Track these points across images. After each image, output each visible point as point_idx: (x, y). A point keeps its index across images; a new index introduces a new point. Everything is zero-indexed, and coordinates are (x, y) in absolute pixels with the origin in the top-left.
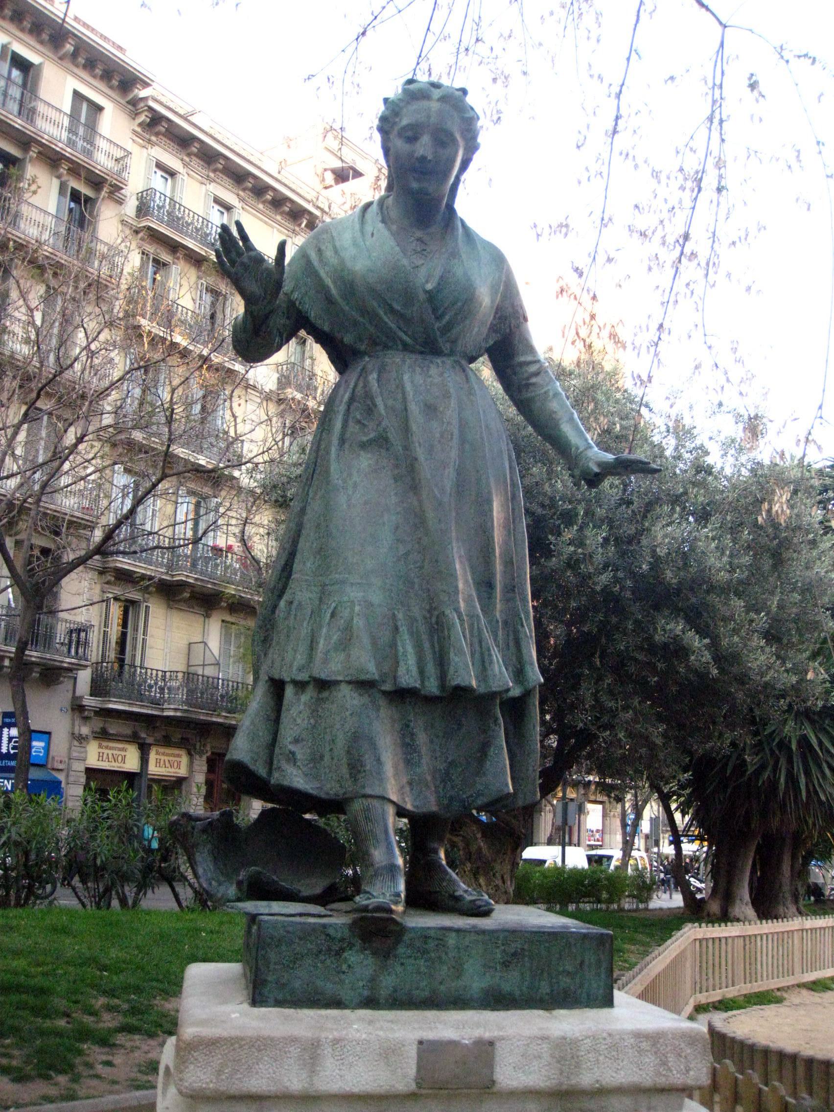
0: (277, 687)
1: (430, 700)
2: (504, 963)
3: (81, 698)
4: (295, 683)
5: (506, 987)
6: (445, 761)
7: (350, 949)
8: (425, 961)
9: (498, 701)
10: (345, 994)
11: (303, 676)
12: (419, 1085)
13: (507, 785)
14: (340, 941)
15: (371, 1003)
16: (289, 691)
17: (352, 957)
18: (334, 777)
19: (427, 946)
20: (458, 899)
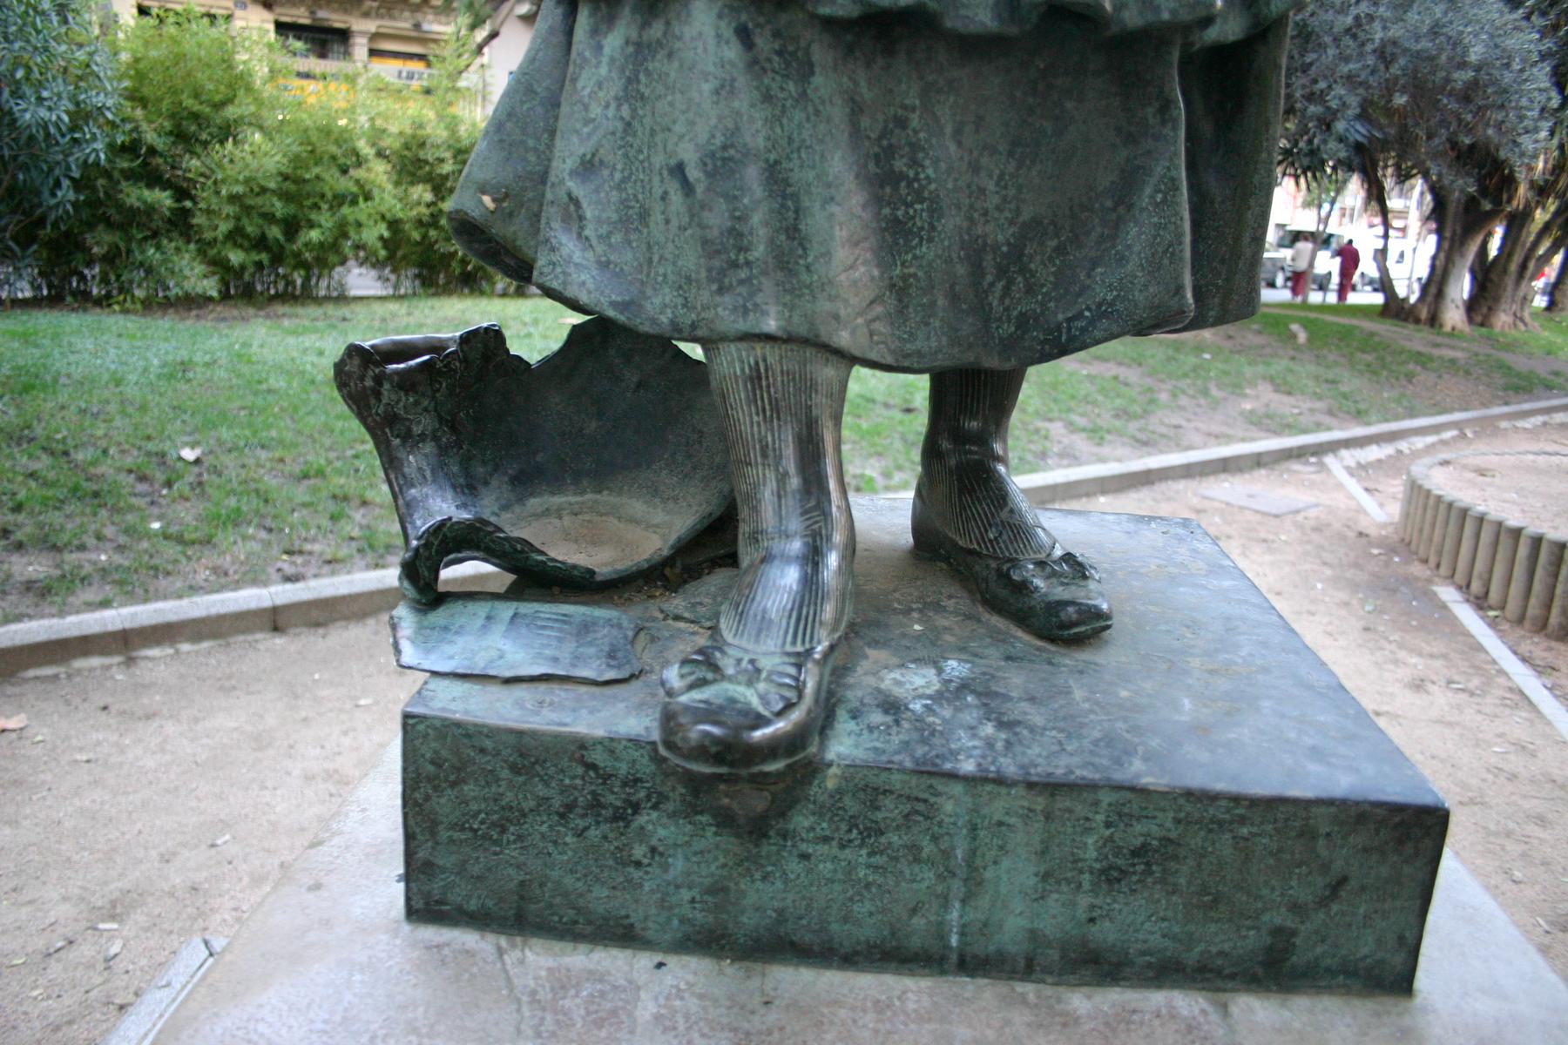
2: (1103, 871)
5: (1106, 933)
6: (1012, 222)
7: (655, 807)
8: (871, 854)
9: (1175, 56)
10: (641, 910)
13: (1179, 289)
14: (625, 784)
17: (658, 826)
18: (671, 277)
19: (879, 816)
20: (1023, 587)
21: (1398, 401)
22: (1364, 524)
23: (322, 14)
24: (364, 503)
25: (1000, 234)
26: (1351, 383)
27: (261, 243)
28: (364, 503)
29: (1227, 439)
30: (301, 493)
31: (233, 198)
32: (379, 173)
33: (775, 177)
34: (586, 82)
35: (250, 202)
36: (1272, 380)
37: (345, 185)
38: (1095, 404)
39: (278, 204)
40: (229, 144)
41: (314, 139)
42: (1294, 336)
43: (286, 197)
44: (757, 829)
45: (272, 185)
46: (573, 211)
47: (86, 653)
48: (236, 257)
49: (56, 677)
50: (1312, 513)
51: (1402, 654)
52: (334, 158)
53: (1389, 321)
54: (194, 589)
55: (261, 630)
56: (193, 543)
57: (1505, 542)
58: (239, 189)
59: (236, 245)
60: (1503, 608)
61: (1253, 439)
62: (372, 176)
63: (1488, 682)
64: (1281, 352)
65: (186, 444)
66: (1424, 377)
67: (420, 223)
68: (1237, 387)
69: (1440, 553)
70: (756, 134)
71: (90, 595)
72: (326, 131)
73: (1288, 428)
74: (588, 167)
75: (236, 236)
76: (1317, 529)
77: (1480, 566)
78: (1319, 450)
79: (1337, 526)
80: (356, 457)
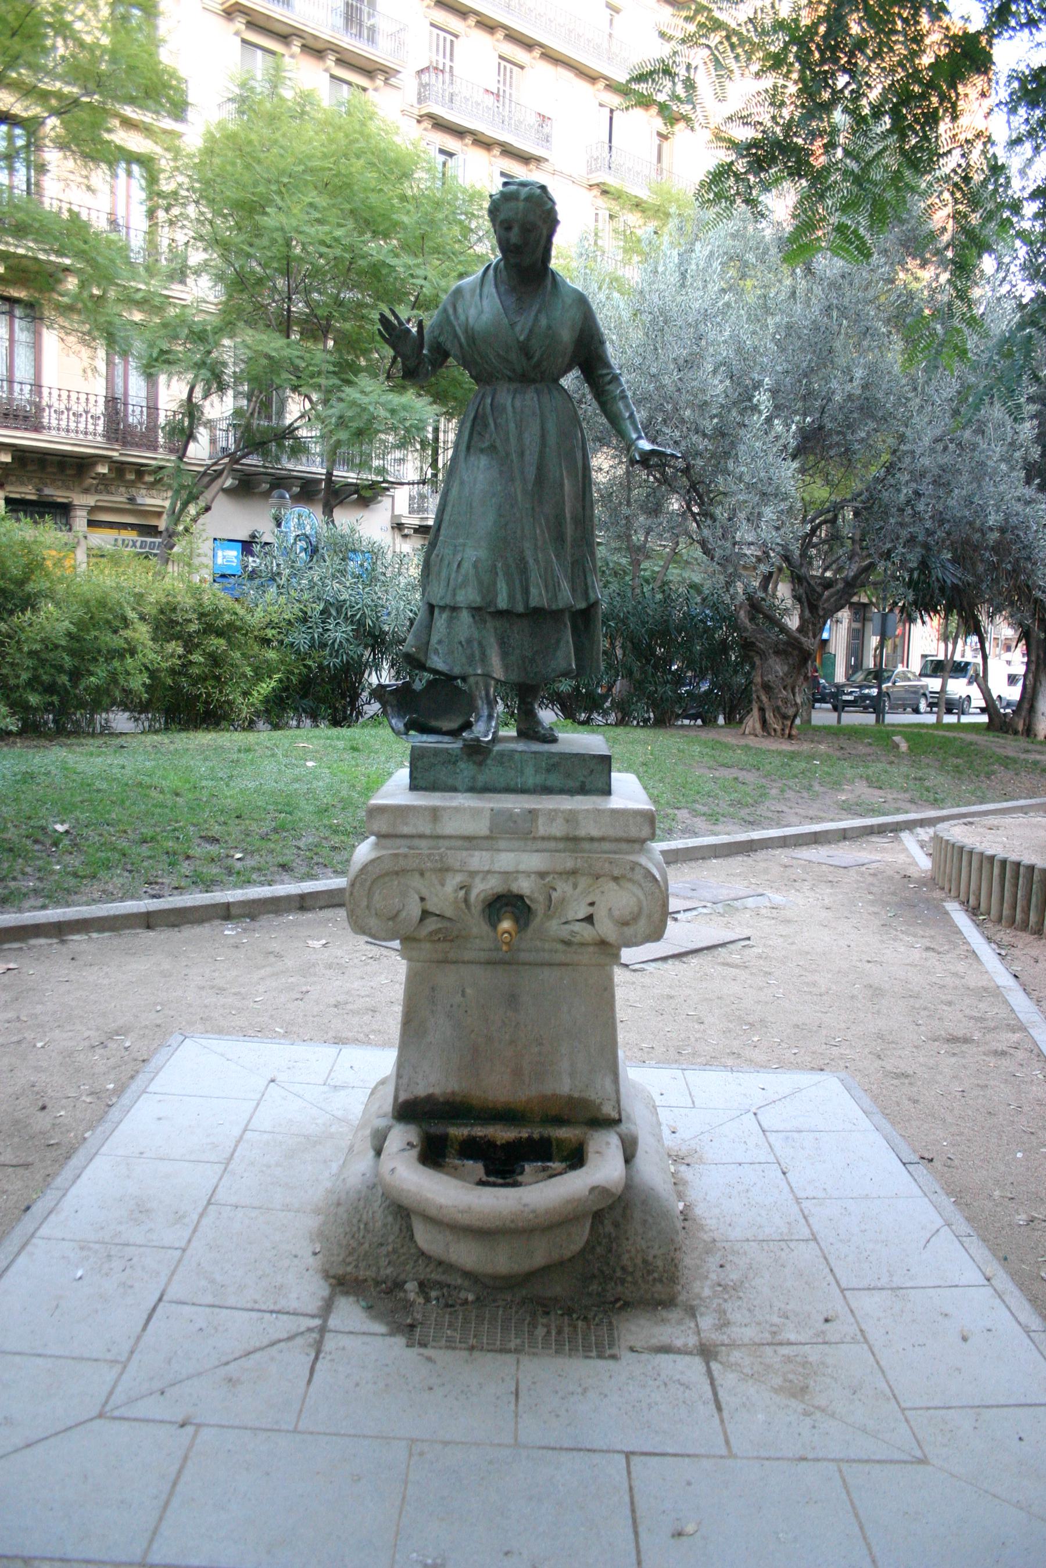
0: (431, 608)
1: (520, 616)
3: (400, 516)
4: (440, 607)
5: (549, 783)
10: (458, 784)
11: (442, 604)
12: (491, 831)
15: (472, 790)
16: (436, 611)
17: (462, 765)
21: (973, 793)
22: (912, 872)
23: (47, 491)
24: (188, 857)
25: (529, 654)
26: (936, 779)
27: (50, 689)
28: (188, 857)
29: (821, 820)
30: (145, 850)
31: (32, 654)
32: (142, 633)
33: (480, 644)
34: (438, 624)
35: (43, 656)
36: (867, 779)
37: (116, 642)
38: (716, 797)
39: (67, 658)
40: (28, 613)
41: (93, 610)
42: (897, 746)
43: (72, 653)
44: (480, 764)
45: (63, 643)
46: (436, 652)
47: (37, 936)
48: (34, 699)
49: (21, 949)
50: (875, 865)
51: (901, 936)
52: (108, 622)
53: (991, 734)
54: (95, 901)
55: (140, 927)
56: (84, 877)
57: (986, 866)
58: (37, 647)
59: (34, 690)
60: (989, 914)
61: (841, 820)
62: (137, 635)
63: (955, 946)
64: (883, 759)
65: (56, 823)
66: (1001, 772)
67: (172, 672)
68: (837, 785)
69: (950, 881)
70: (476, 635)
71: (32, 902)
72: (102, 604)
73: (873, 812)
74: (440, 642)
75: (33, 683)
76: (874, 875)
77: (973, 886)
78: (897, 828)
79: (890, 872)
80: (174, 830)
